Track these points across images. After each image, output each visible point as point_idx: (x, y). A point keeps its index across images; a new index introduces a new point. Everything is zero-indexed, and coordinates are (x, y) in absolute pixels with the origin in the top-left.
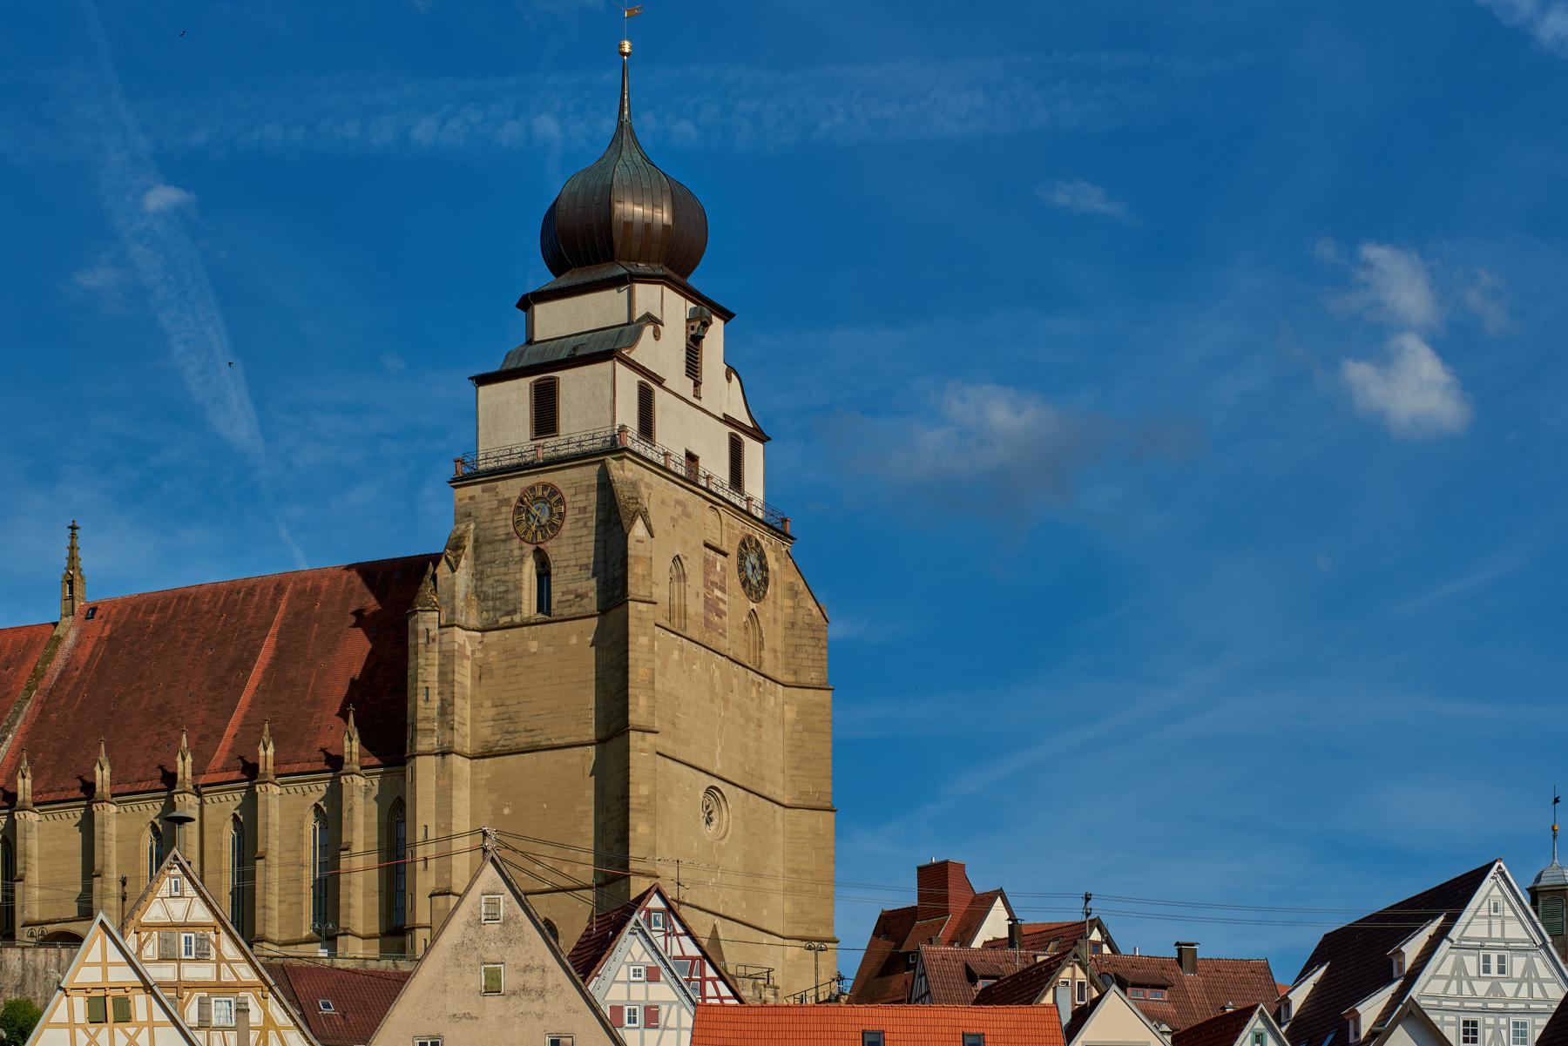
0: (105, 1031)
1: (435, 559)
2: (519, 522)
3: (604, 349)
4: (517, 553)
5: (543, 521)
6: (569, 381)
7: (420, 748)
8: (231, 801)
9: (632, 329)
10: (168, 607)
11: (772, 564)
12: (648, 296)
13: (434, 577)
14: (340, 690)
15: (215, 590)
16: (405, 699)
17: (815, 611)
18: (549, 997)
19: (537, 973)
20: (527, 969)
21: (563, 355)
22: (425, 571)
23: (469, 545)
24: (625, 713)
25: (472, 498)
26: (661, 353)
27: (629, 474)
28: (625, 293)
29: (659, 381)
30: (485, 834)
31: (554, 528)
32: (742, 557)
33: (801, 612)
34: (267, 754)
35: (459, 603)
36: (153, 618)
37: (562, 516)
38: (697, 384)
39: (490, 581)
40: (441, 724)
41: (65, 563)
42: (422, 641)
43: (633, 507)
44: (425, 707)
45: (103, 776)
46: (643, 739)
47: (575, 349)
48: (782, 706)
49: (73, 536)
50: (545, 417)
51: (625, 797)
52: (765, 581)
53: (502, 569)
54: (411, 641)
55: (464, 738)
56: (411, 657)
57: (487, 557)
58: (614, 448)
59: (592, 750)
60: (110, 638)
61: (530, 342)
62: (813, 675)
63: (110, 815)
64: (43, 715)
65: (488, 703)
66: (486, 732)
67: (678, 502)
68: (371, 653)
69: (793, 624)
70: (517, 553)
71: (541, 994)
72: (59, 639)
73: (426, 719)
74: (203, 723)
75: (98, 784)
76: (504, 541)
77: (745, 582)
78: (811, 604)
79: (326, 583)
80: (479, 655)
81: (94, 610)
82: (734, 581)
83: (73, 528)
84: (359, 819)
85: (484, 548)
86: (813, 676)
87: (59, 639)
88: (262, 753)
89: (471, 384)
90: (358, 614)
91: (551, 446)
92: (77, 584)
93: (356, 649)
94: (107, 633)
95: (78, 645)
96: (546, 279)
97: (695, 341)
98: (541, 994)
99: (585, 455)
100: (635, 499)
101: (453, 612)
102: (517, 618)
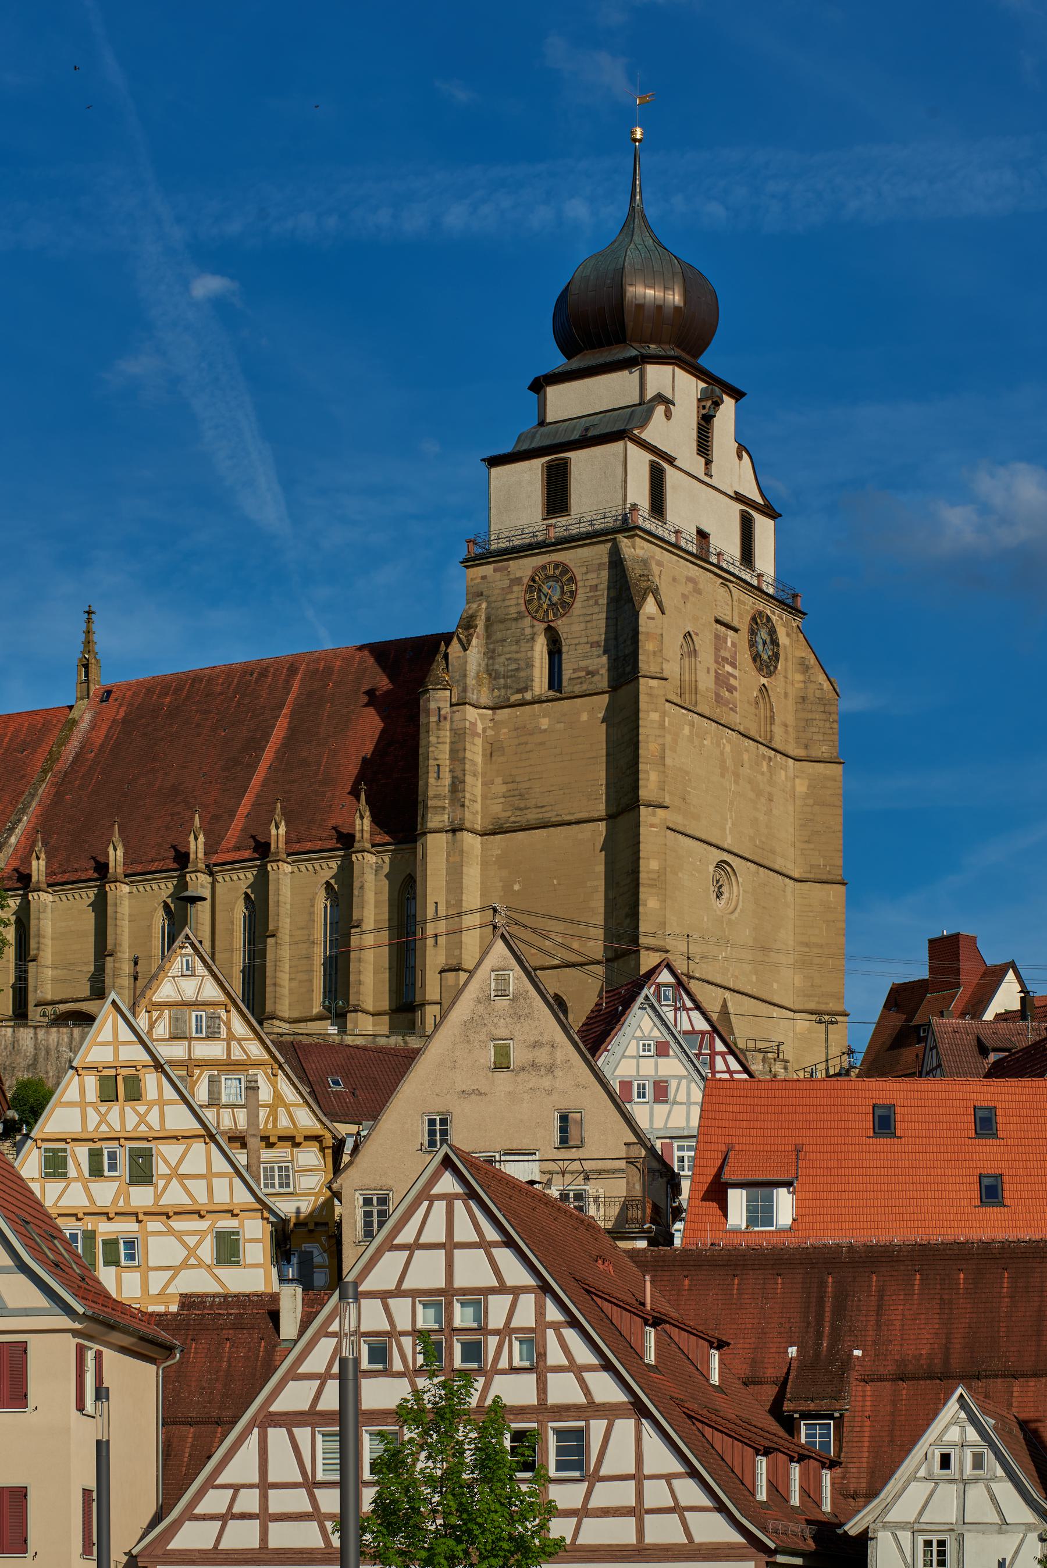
0: (115, 1109)
2: (530, 601)
3: (617, 429)
4: (528, 631)
6: (582, 463)
7: (431, 825)
8: (243, 880)
9: (643, 409)
11: (783, 639)
12: (660, 377)
13: (446, 656)
14: (352, 769)
17: (826, 685)
18: (558, 1073)
19: (547, 1049)
20: (536, 1045)
21: (575, 436)
23: (481, 623)
25: (484, 578)
26: (672, 431)
27: (639, 552)
29: (671, 460)
30: (495, 910)
31: (565, 606)
32: (753, 632)
33: (812, 687)
34: (278, 833)
35: (471, 681)
36: (168, 700)
37: (573, 594)
38: (708, 463)
39: (502, 659)
40: (453, 801)
42: (433, 719)
44: (436, 785)
45: (116, 857)
46: (654, 815)
47: (587, 429)
48: (793, 780)
49: (89, 621)
50: (557, 496)
51: (635, 872)
52: (776, 656)
53: (514, 648)
54: (423, 720)
55: (475, 815)
56: (422, 735)
57: (499, 635)
58: (627, 527)
59: (602, 826)
60: (125, 721)
61: (542, 423)
62: (824, 749)
63: (121, 894)
64: (58, 797)
65: (499, 780)
67: (689, 579)
68: (383, 732)
69: (804, 699)
70: (528, 631)
71: (550, 1069)
72: (74, 722)
73: (436, 796)
75: (111, 864)
76: (516, 620)
77: (756, 657)
78: (821, 678)
79: (338, 663)
80: (490, 732)
81: (109, 692)
82: (745, 657)
83: (89, 613)
84: (370, 896)
85: (495, 627)
86: (823, 750)
87: (74, 722)
88: (274, 831)
89: (483, 466)
90: (370, 693)
91: (562, 526)
92: (92, 669)
94: (122, 714)
95: (93, 726)
96: (558, 361)
97: (705, 422)
98: (550, 1069)
100: (646, 577)
101: (465, 690)
102: (528, 696)
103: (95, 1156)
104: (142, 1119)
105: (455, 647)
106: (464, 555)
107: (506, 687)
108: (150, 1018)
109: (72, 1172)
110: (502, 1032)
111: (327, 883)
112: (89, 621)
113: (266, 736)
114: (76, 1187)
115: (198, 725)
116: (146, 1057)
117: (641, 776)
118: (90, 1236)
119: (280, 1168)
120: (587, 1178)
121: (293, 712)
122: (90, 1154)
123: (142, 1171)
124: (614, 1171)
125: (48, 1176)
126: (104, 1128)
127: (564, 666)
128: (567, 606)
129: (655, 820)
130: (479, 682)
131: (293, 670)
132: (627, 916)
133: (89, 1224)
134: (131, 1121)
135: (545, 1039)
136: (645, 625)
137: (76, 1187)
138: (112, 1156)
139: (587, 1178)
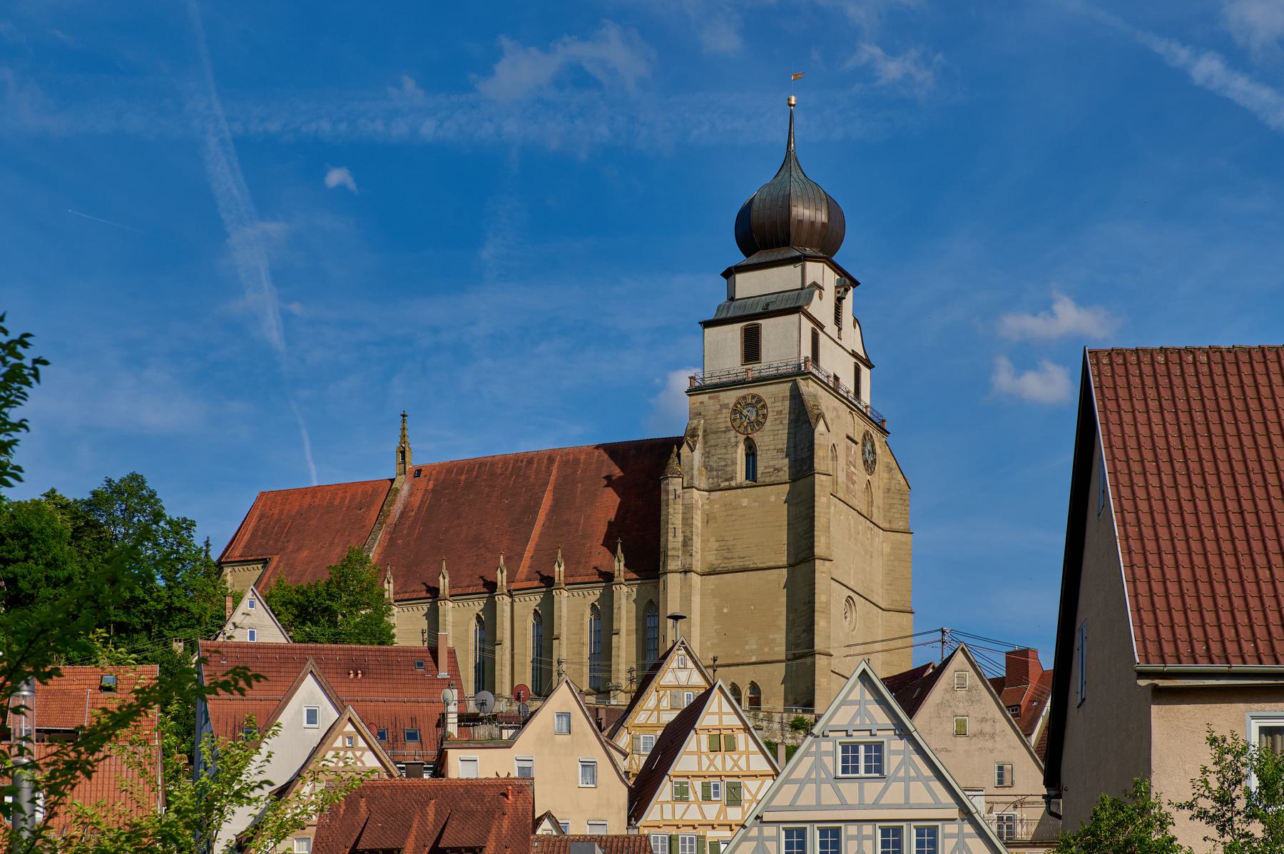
0: (719, 756)
1: (679, 442)
2: (735, 420)
4: (733, 440)
5: (753, 418)
6: (768, 327)
7: (670, 568)
8: (533, 601)
11: (878, 451)
12: (817, 271)
13: (679, 456)
14: (602, 529)
15: (505, 460)
17: (902, 481)
18: (997, 738)
19: (990, 723)
20: (983, 720)
21: (759, 310)
22: (671, 451)
23: (700, 433)
24: (812, 547)
25: (702, 403)
26: (822, 307)
27: (811, 390)
28: (799, 268)
29: (821, 327)
30: (943, 632)
32: (864, 445)
33: (894, 482)
34: (559, 571)
35: (695, 473)
37: (765, 416)
38: (840, 329)
40: (684, 552)
42: (671, 497)
44: (673, 542)
45: (444, 583)
47: (768, 305)
48: (882, 543)
49: (404, 421)
50: (752, 350)
52: (874, 462)
54: (663, 497)
56: (663, 507)
57: (712, 442)
58: (800, 373)
59: (785, 571)
60: (433, 491)
61: (732, 299)
63: (448, 609)
64: (392, 540)
65: (713, 539)
66: (712, 558)
67: (835, 409)
68: (620, 504)
70: (733, 440)
71: (992, 736)
72: (397, 490)
73: (673, 549)
75: (441, 588)
77: (865, 462)
78: (900, 476)
79: (583, 457)
80: (707, 507)
82: (860, 462)
84: (624, 613)
85: (710, 436)
87: (397, 490)
88: (557, 569)
89: (700, 327)
90: (608, 478)
91: (756, 369)
92: (407, 454)
93: (610, 503)
94: (431, 486)
95: (411, 494)
96: (740, 258)
97: (839, 300)
98: (992, 736)
100: (817, 406)
102: (733, 484)
103: (706, 787)
104: (736, 764)
105: (685, 450)
106: (687, 386)
107: (717, 477)
109: (692, 798)
110: (961, 711)
111: (593, 605)
112: (404, 421)
113: (538, 504)
114: (694, 807)
116: (739, 723)
118: (701, 839)
119: (856, 770)
120: (1015, 807)
121: (555, 489)
123: (734, 798)
124: (1033, 803)
125: (677, 800)
126: (712, 769)
127: (758, 464)
128: (760, 424)
129: (824, 569)
130: (700, 473)
133: (701, 831)
134: (729, 764)
135: (989, 716)
136: (818, 439)
137: (694, 807)
138: (716, 787)
139: (1015, 807)
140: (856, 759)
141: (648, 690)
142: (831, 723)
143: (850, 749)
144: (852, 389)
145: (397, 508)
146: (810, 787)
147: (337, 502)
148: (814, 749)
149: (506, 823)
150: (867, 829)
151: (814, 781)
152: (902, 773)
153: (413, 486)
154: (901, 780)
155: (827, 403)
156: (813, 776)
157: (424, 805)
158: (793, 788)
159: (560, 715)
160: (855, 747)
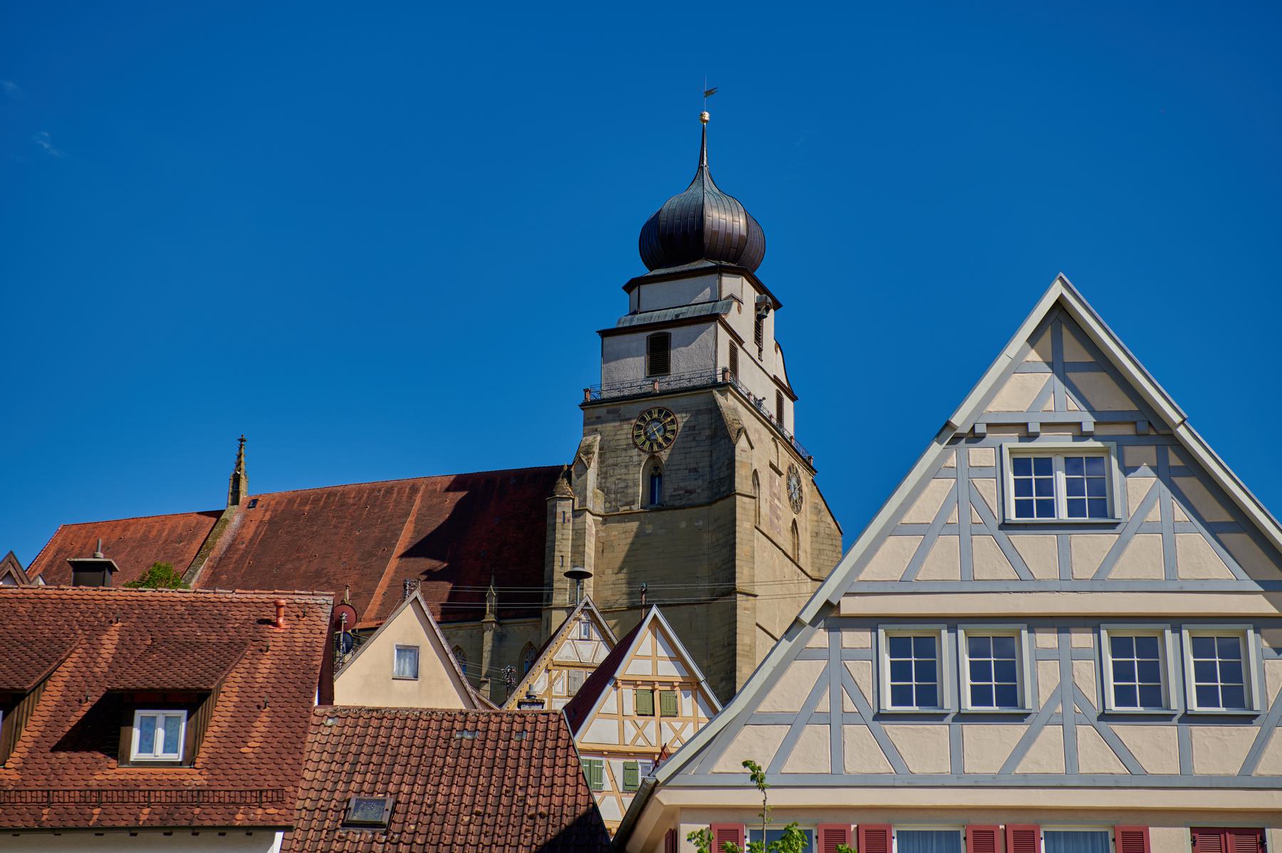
0: (653, 723)
4: (636, 459)
10: (319, 500)
11: (805, 489)
12: (733, 284)
16: (543, 565)
17: (833, 525)
24: (732, 578)
26: (742, 320)
29: (741, 342)
32: (789, 479)
35: (589, 494)
36: (307, 508)
38: (760, 350)
41: (234, 466)
42: (559, 520)
43: (738, 426)
47: (677, 316)
50: (659, 363)
53: (623, 471)
54: (549, 521)
57: (611, 461)
60: (271, 521)
65: (610, 571)
70: (636, 459)
72: (226, 521)
74: (356, 584)
76: (625, 450)
78: (830, 519)
81: (255, 502)
82: (785, 497)
83: (242, 440)
87: (226, 521)
95: (243, 526)
96: (644, 271)
97: (760, 318)
99: (694, 388)
100: (738, 421)
101: (585, 500)
106: (581, 401)
107: (616, 500)
108: (550, 677)
115: (335, 527)
117: (737, 570)
121: (417, 520)
122: (625, 768)
126: (641, 741)
129: (748, 604)
131: (414, 489)
132: (722, 680)
140: (1046, 488)
141: (536, 669)
142: (992, 407)
143: (1032, 469)
144: (775, 415)
145: (223, 542)
146: (947, 546)
147: (154, 533)
148: (952, 461)
149: (266, 665)
150: (1082, 639)
151: (826, 719)
152: (1155, 515)
153: (246, 516)
154: (1152, 529)
155: (748, 420)
156: (954, 518)
157: (96, 631)
158: (913, 543)
159: (402, 650)
160: (1045, 466)
